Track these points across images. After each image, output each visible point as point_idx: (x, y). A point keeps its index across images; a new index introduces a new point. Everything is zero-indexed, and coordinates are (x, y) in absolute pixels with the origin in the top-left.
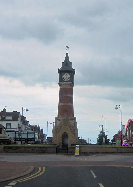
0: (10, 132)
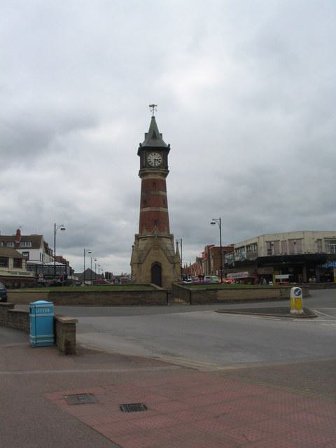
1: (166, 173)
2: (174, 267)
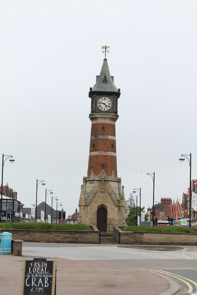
1: (115, 118)
2: (120, 210)
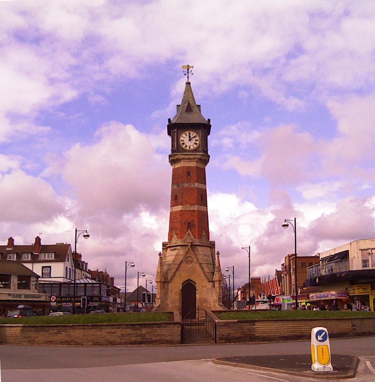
0: (68, 285)
1: (205, 160)
